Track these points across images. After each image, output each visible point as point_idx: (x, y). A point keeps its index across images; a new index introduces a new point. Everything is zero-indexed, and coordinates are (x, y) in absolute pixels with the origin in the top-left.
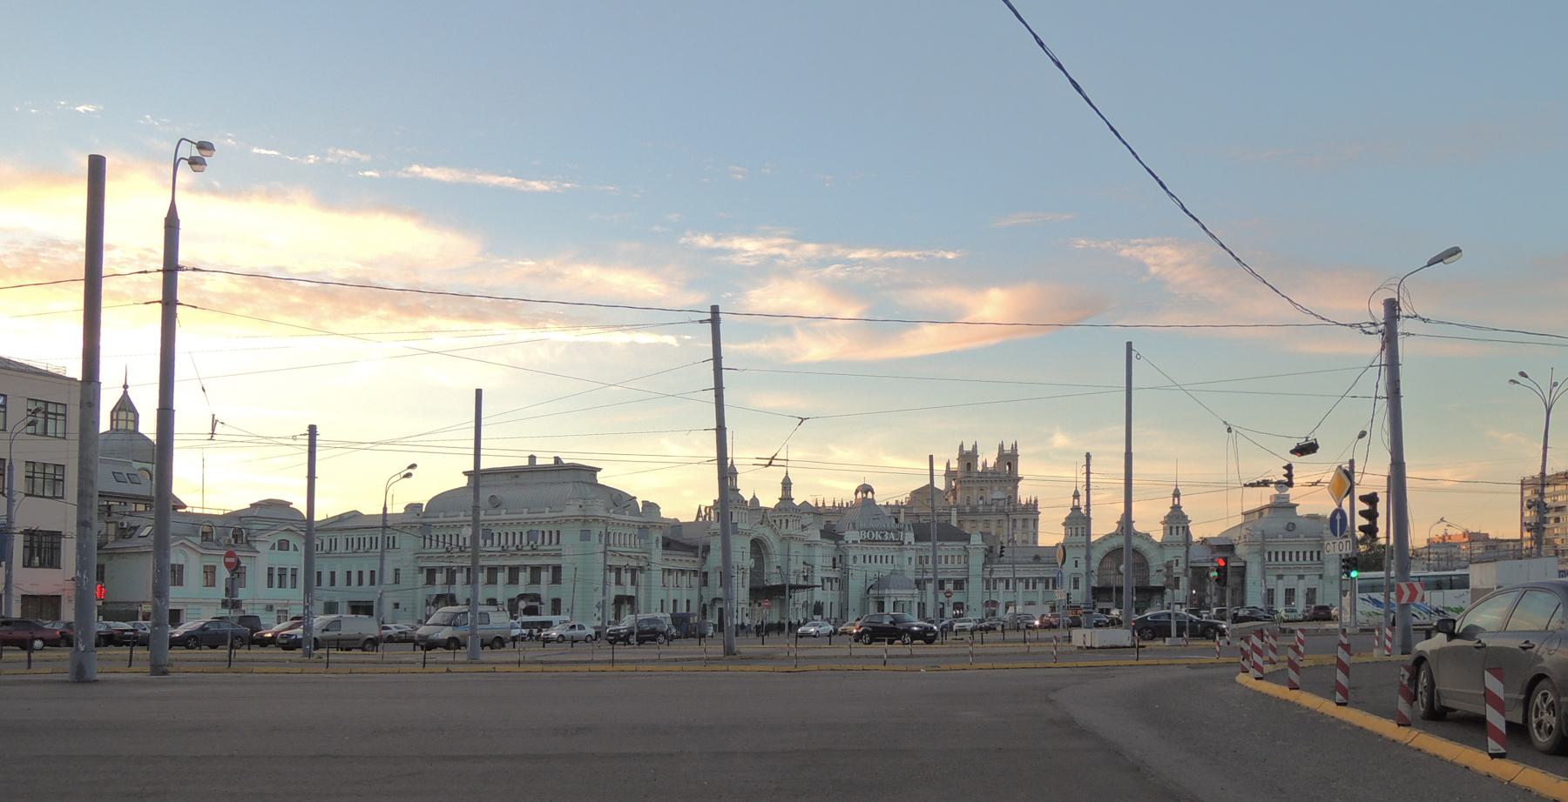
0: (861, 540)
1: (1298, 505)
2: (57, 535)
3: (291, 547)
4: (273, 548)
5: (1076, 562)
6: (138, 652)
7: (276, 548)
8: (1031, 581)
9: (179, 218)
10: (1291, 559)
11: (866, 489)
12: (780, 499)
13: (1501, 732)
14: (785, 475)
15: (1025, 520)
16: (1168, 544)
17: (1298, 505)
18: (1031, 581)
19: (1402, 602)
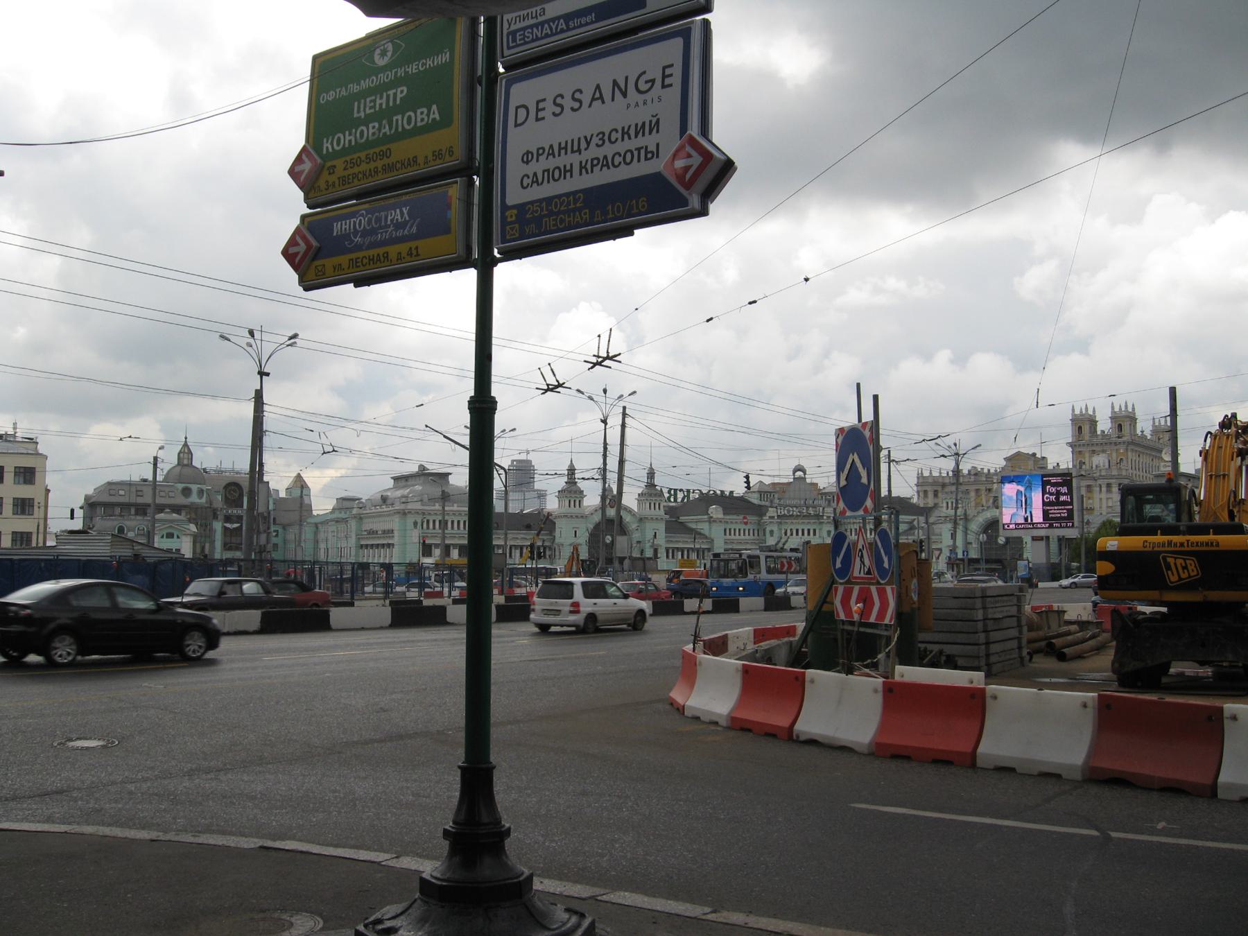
0: (778, 516)
1: (451, 474)
2: (31, 533)
3: (175, 536)
4: (162, 537)
5: (576, 532)
6: (703, 619)
7: (165, 537)
8: (671, 551)
9: (618, 240)
10: (459, 528)
11: (799, 468)
12: (566, 483)
13: (5, 662)
14: (570, 462)
15: (1089, 487)
16: (413, 512)
17: (451, 474)
18: (671, 551)
19: (837, 567)
